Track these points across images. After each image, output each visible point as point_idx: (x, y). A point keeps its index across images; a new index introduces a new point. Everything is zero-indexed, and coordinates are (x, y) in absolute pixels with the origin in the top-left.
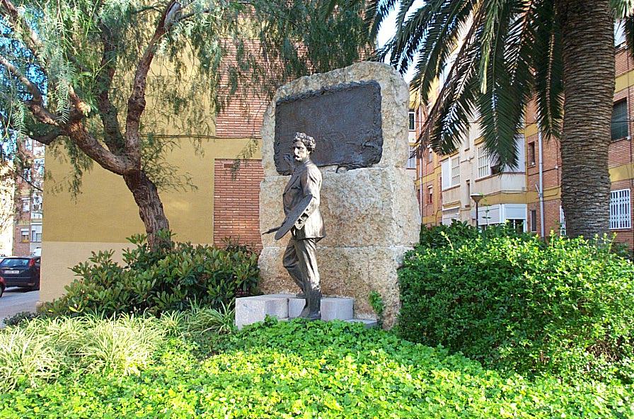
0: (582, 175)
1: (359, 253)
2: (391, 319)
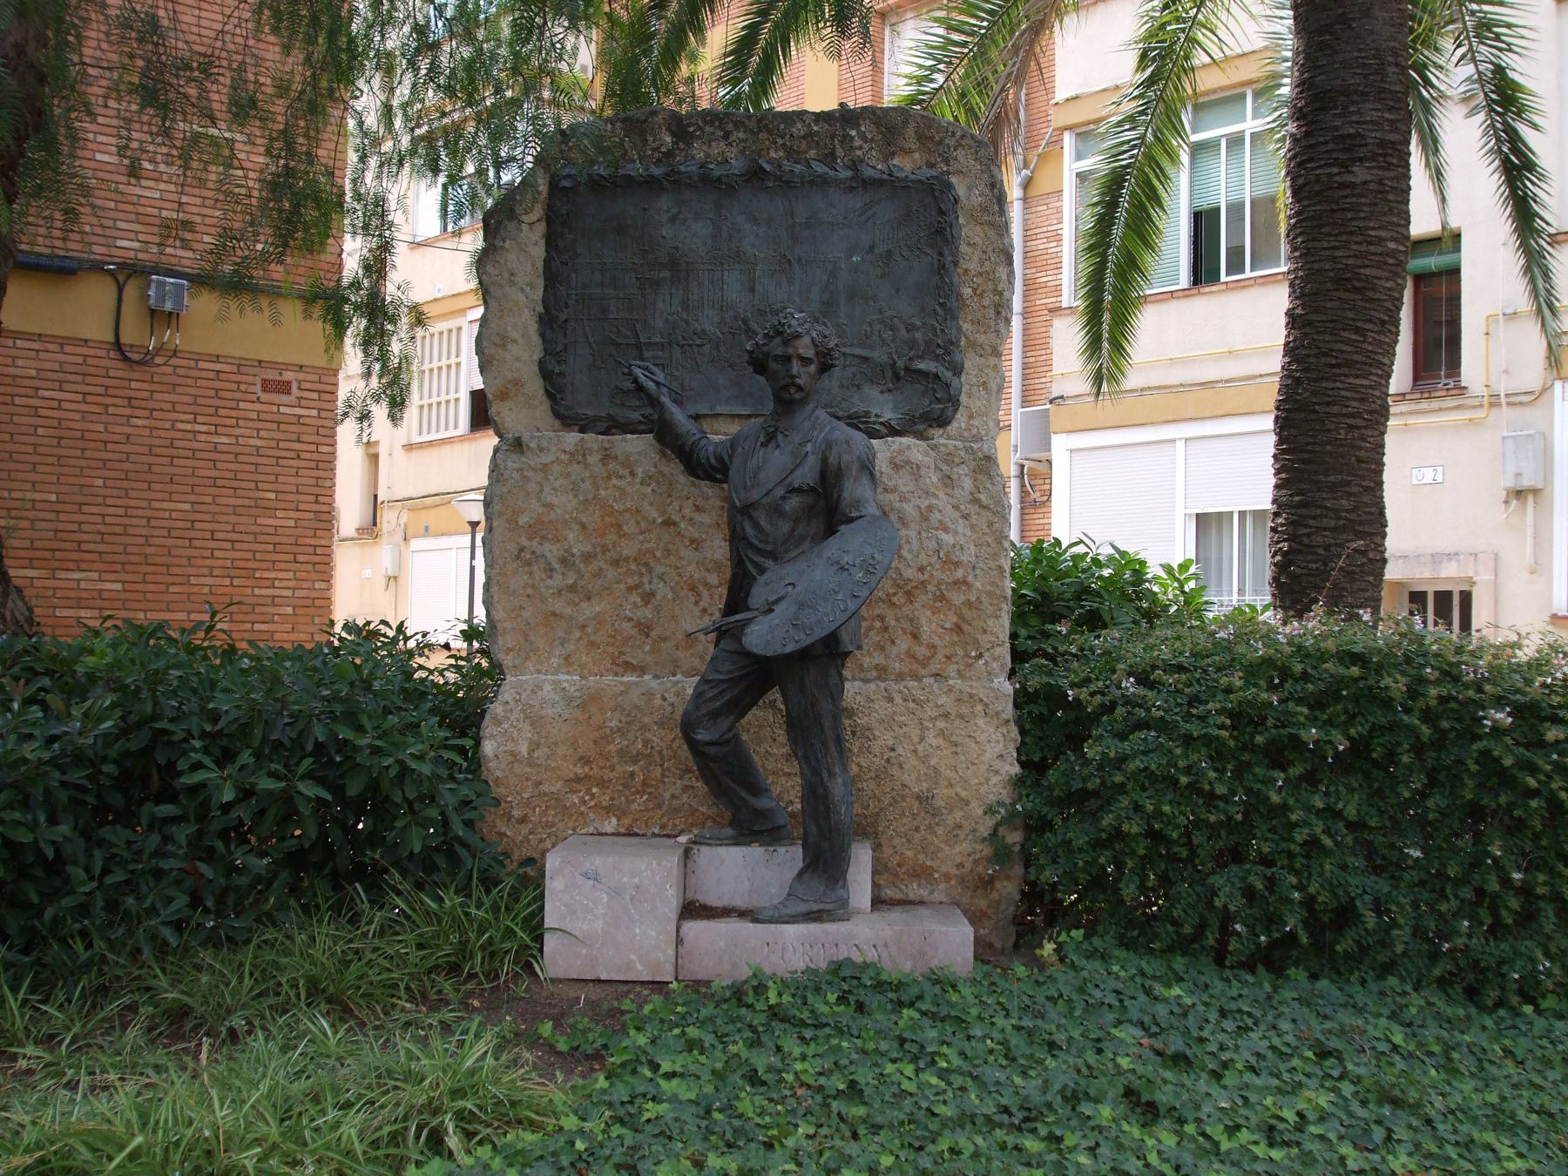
2: (995, 895)
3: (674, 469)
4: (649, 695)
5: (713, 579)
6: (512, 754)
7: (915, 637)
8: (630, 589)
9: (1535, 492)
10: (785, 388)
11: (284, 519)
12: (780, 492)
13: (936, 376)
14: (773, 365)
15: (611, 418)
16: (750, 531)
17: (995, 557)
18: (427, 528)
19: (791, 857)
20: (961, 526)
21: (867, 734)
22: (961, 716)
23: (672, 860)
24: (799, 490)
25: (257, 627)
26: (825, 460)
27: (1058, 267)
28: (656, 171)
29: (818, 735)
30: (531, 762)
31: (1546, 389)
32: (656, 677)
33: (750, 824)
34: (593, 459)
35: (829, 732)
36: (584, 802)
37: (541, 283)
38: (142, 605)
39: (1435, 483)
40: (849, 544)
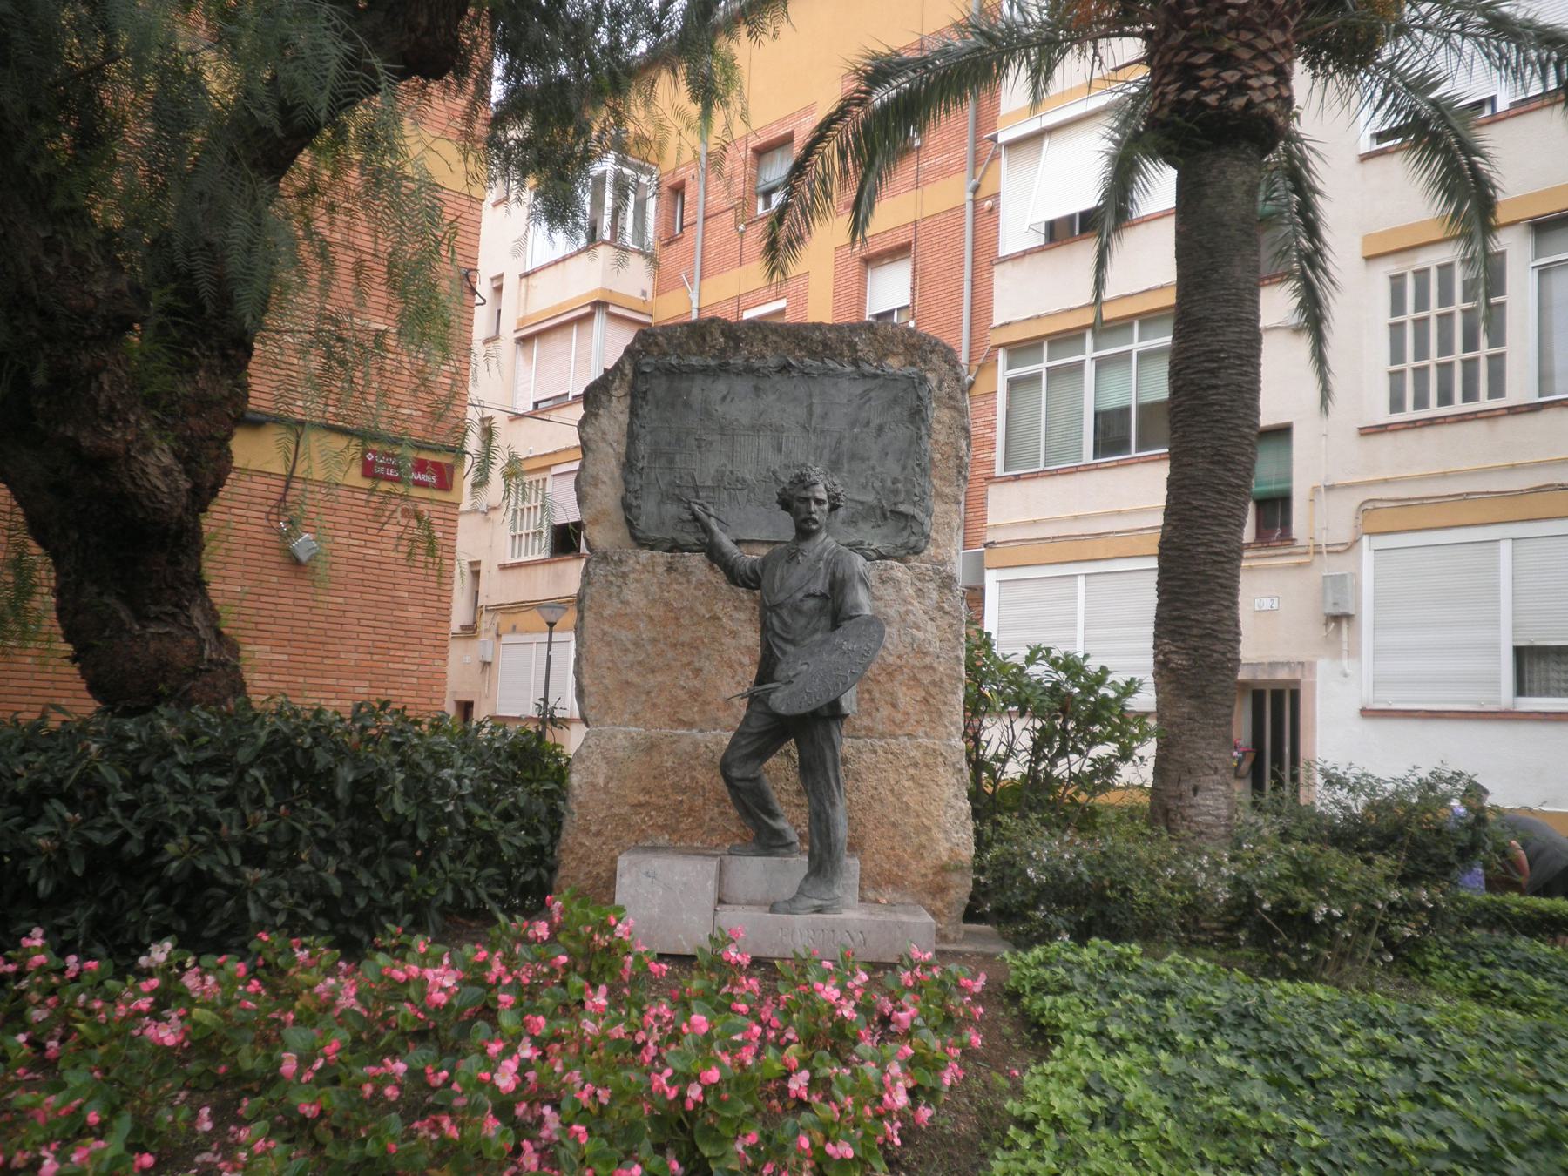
0: (1210, 617)
1: (875, 752)
3: (719, 579)
4: (696, 745)
5: (746, 660)
6: (593, 785)
7: (894, 706)
8: (684, 666)
9: (1348, 617)
10: (805, 521)
11: (412, 612)
12: (800, 595)
13: (913, 517)
14: (796, 504)
15: (673, 540)
16: (775, 622)
17: (954, 649)
18: (514, 628)
19: (799, 864)
20: (931, 626)
21: (857, 777)
22: (927, 766)
23: (712, 866)
24: (814, 596)
25: (390, 692)
26: (833, 574)
27: (992, 447)
28: (712, 363)
29: (817, 773)
30: (606, 790)
31: (1356, 541)
32: (701, 731)
33: (769, 842)
34: (660, 570)
35: (831, 774)
36: (644, 822)
37: (624, 441)
38: (303, 672)
39: (1271, 610)
40: (845, 639)
